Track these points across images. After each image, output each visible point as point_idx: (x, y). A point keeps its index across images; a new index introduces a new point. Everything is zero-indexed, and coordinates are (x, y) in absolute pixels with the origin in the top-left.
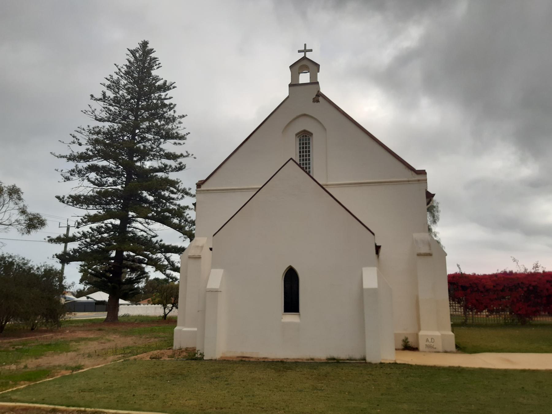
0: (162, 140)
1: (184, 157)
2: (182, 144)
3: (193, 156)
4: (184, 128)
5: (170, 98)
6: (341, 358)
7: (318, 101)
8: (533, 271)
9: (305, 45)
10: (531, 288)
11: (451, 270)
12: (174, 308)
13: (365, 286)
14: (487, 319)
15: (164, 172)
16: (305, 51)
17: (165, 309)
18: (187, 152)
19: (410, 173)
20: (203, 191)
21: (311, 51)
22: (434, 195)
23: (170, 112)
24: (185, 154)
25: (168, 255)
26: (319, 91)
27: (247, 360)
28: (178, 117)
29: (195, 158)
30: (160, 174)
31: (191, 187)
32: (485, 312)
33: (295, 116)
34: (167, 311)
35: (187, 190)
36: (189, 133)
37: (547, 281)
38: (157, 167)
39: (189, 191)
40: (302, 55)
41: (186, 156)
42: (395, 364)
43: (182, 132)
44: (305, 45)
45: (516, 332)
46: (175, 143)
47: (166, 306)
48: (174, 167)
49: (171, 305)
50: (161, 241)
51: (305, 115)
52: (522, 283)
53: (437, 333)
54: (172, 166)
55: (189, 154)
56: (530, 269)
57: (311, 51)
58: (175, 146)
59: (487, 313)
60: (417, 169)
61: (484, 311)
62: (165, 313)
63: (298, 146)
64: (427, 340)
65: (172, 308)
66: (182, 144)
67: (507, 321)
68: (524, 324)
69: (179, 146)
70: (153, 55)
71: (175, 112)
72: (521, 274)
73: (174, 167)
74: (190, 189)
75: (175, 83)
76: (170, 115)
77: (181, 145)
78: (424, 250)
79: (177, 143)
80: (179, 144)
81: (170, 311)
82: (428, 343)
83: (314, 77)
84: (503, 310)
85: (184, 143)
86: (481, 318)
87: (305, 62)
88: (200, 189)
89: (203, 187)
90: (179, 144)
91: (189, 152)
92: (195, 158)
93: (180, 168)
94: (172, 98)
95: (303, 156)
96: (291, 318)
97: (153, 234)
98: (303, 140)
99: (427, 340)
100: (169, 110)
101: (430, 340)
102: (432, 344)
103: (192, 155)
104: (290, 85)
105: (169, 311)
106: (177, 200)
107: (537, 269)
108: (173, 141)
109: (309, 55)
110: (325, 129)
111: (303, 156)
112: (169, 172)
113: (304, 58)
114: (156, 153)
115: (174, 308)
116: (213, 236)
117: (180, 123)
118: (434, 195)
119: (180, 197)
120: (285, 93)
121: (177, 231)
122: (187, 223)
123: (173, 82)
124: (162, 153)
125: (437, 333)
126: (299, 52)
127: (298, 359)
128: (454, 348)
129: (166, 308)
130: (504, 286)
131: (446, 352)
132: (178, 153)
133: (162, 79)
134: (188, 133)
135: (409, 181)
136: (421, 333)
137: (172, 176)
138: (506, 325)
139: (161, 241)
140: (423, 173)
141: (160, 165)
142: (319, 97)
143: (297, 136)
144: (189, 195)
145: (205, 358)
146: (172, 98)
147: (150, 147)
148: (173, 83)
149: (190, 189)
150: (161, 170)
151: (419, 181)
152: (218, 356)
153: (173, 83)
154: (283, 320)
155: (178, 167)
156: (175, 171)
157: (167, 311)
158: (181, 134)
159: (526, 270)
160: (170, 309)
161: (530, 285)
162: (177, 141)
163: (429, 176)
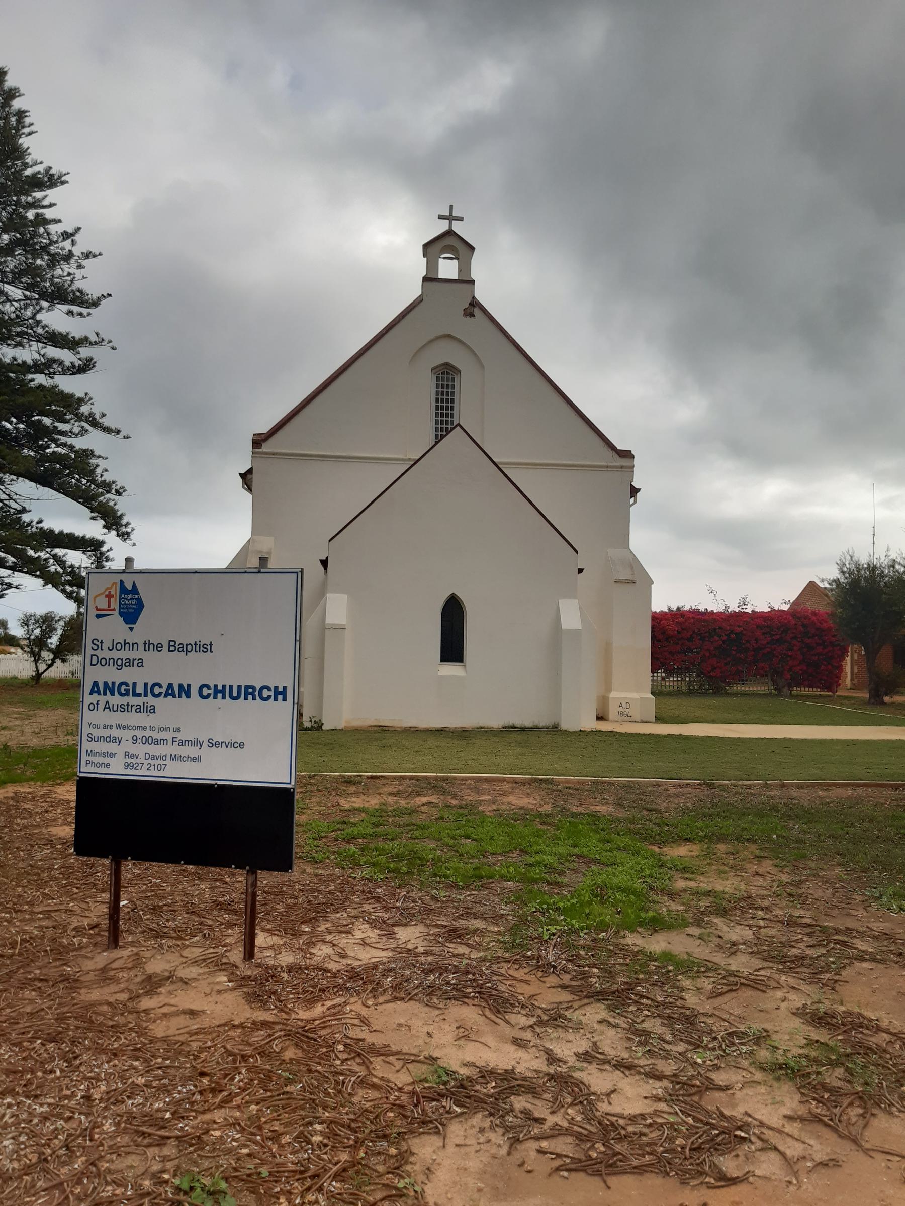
0: (45, 304)
1: (91, 344)
2: (86, 314)
3: (110, 344)
4: (84, 278)
5: (51, 205)
6: (527, 726)
7: (472, 315)
8: (737, 610)
9: (451, 206)
10: (733, 636)
11: (661, 602)
12: (58, 661)
13: (565, 626)
14: (663, 683)
15: (46, 374)
16: (450, 218)
17: (36, 662)
18: (97, 334)
19: (610, 453)
20: (266, 453)
21: (461, 219)
22: (639, 490)
23: (63, 243)
24: (93, 338)
25: (59, 551)
26: (474, 297)
27: (386, 728)
28: (81, 256)
29: (113, 348)
30: (40, 379)
31: (105, 412)
32: (661, 673)
33: (432, 337)
34: (42, 667)
35: (97, 416)
36: (110, 295)
37: (758, 626)
38: (30, 362)
39: (100, 420)
40: (443, 226)
41: (96, 343)
42: (600, 731)
43: (92, 290)
44: (451, 206)
45: (714, 701)
46: (70, 313)
47: (40, 655)
48: (67, 364)
49: (52, 656)
50: (40, 521)
51: (449, 336)
52: (720, 628)
53: (636, 696)
54: (65, 363)
55: (103, 340)
56: (734, 607)
57: (461, 219)
58: (69, 318)
59: (663, 675)
60: (619, 448)
61: (659, 671)
62: (38, 670)
63: (434, 390)
64: (621, 705)
65: (53, 661)
66: (86, 314)
67: (692, 688)
68: (718, 691)
69: (78, 319)
70: (17, 104)
71: (73, 243)
72: (719, 613)
73: (67, 364)
74: (103, 415)
75: (68, 174)
76: (61, 249)
77: (85, 317)
78: (625, 575)
79: (75, 311)
80: (80, 314)
81: (50, 666)
82: (621, 709)
83: (465, 267)
84: (688, 670)
85: (89, 314)
86: (677, 677)
87: (450, 241)
88: (260, 450)
89: (266, 447)
90: (80, 314)
91: (102, 335)
92: (113, 348)
93: (86, 367)
94: (54, 204)
95: (442, 408)
96: (451, 670)
97: (19, 508)
98: (443, 381)
99: (621, 705)
100: (64, 238)
101: (624, 706)
102: (627, 710)
103: (110, 342)
104: (425, 279)
105: (45, 667)
106: (71, 437)
107: (744, 607)
108: (66, 307)
109: (457, 227)
110: (482, 367)
111: (442, 408)
112: (54, 373)
113: (450, 233)
114: (26, 329)
115: (58, 661)
116: (330, 541)
117: (80, 267)
118: (639, 490)
119: (76, 430)
120: (415, 291)
121: (79, 502)
122: (93, 486)
123: (64, 173)
124: (40, 330)
125: (636, 696)
126: (439, 218)
127: (455, 728)
128: (653, 719)
129: (39, 659)
130: (694, 632)
131: (642, 722)
132: (77, 334)
133: (41, 163)
134: (105, 295)
135: (607, 467)
136: (613, 695)
137: (68, 384)
138: (690, 693)
139: (40, 521)
140: (627, 455)
141: (37, 356)
142: (474, 307)
143: (433, 372)
144: (100, 427)
145: (324, 728)
146: (54, 204)
147: (13, 316)
148: (65, 175)
149: (103, 415)
150: (37, 368)
151: (622, 467)
152: (341, 725)
153: (65, 175)
154: (440, 673)
155: (77, 365)
156: (70, 375)
157: (42, 667)
158: (90, 296)
159: (727, 607)
160: (50, 662)
161: (732, 632)
162: (76, 309)
163: (637, 461)
